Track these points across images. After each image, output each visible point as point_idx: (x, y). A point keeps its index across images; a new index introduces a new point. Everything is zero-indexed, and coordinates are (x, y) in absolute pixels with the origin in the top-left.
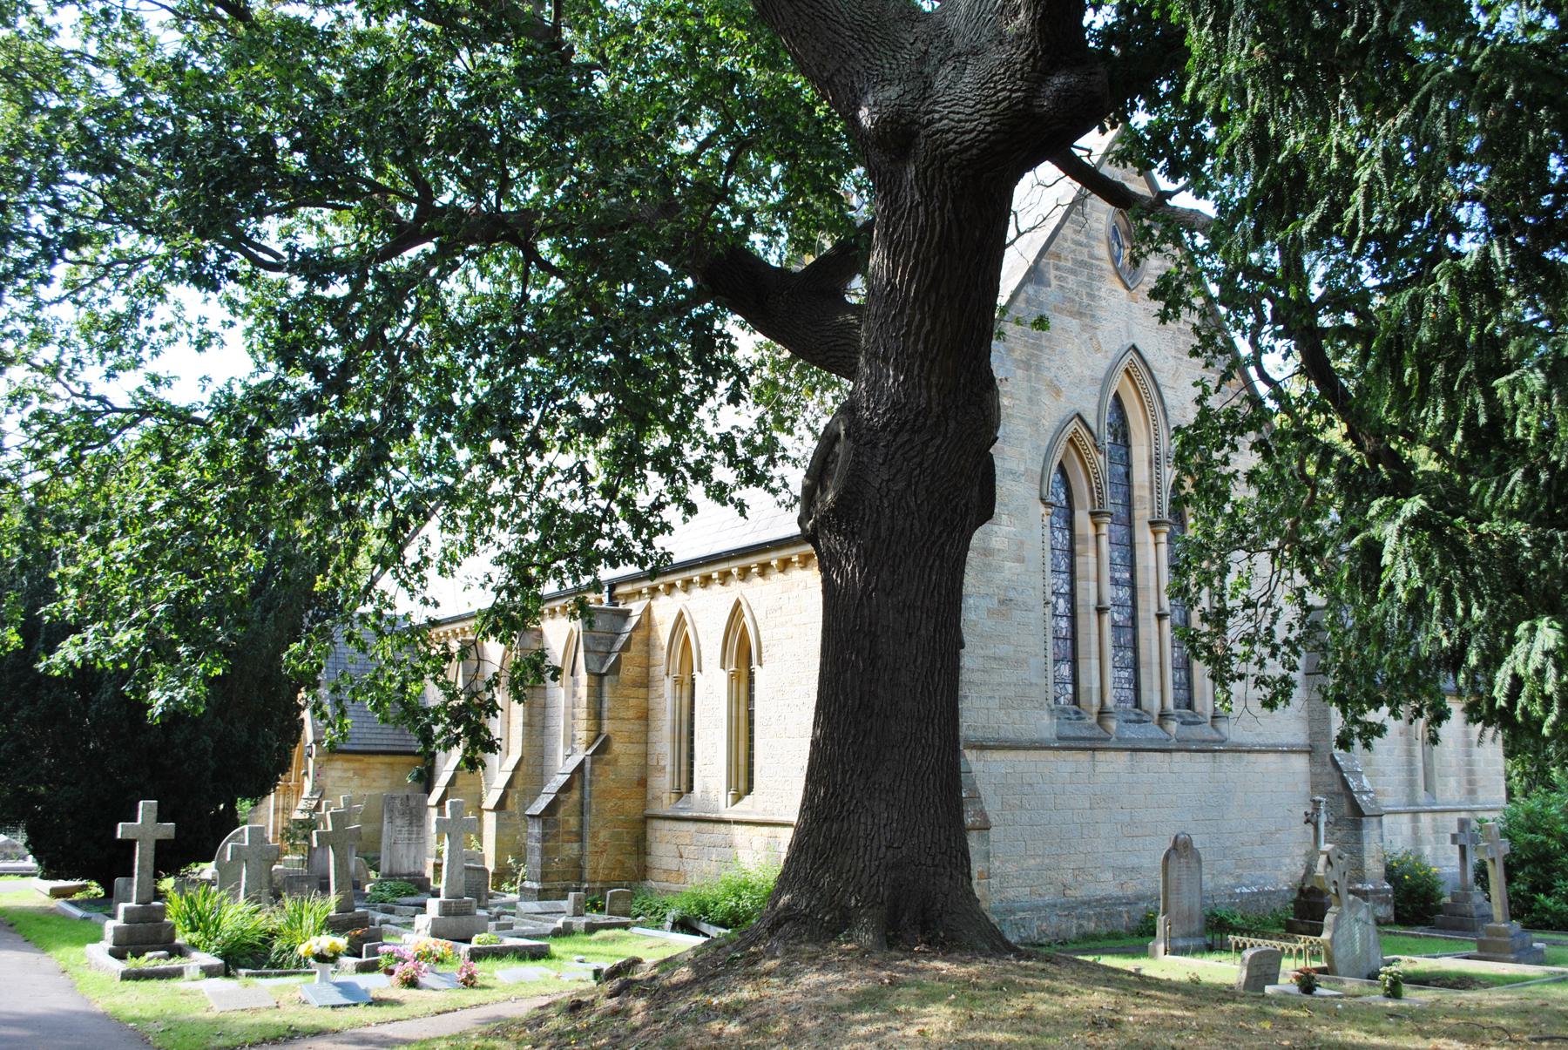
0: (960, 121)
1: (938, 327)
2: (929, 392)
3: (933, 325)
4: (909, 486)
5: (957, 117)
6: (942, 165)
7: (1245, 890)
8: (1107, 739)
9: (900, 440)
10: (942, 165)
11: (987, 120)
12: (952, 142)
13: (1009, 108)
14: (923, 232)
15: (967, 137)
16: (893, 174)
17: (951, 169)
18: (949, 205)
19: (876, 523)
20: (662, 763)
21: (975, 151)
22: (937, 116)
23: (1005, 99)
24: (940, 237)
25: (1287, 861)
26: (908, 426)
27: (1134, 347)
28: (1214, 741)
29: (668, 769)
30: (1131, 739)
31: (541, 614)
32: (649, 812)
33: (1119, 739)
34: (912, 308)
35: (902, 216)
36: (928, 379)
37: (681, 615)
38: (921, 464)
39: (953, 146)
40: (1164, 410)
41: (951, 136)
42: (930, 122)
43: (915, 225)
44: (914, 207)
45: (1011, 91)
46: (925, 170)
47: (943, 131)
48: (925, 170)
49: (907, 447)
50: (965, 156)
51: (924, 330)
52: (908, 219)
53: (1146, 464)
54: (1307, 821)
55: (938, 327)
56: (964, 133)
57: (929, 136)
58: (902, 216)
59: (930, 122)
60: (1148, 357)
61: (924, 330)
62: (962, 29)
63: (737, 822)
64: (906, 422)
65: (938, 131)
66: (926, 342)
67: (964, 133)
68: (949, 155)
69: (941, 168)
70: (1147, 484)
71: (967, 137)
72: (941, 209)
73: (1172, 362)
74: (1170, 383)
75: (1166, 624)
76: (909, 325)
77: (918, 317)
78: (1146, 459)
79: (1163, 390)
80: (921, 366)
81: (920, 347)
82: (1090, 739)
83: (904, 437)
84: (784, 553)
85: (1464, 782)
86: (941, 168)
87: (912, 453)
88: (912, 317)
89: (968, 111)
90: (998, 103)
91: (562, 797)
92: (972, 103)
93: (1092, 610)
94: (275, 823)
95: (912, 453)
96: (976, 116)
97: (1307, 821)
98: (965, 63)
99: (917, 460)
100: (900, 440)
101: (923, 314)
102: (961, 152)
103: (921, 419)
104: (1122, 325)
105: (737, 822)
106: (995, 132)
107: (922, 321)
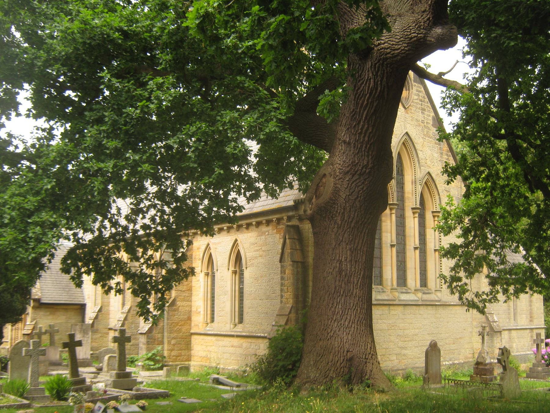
0: (393, 45)
1: (374, 131)
2: (368, 158)
3: (372, 130)
4: (358, 197)
5: (392, 43)
6: (383, 62)
7: (447, 363)
8: (395, 300)
9: (354, 178)
10: (383, 62)
11: (405, 45)
12: (389, 53)
13: (417, 40)
14: (372, 91)
15: (396, 52)
16: (360, 65)
17: (387, 64)
18: (385, 79)
19: (343, 213)
20: (199, 310)
21: (399, 57)
22: (382, 42)
23: (415, 37)
24: (379, 93)
25: (463, 351)
26: (358, 172)
27: (407, 133)
28: (436, 301)
29: (202, 313)
30: (404, 300)
31: (28, 230)
32: (192, 331)
33: (400, 300)
34: (364, 122)
35: (363, 83)
36: (368, 152)
37: (208, 245)
38: (363, 189)
39: (389, 55)
40: (419, 160)
41: (389, 50)
42: (379, 44)
43: (369, 87)
44: (369, 79)
45: (418, 34)
46: (376, 64)
47: (385, 48)
48: (376, 64)
49: (357, 181)
50: (395, 59)
51: (369, 132)
52: (366, 84)
53: (410, 183)
54: (480, 335)
55: (374, 131)
56: (394, 50)
57: (378, 50)
58: (363, 83)
59: (379, 44)
60: (412, 137)
61: (369, 132)
62: (393, 5)
63: (232, 336)
64: (358, 170)
65: (383, 48)
66: (369, 137)
67: (394, 50)
68: (387, 59)
69: (383, 64)
70: (411, 192)
71: (396, 52)
72: (381, 81)
73: (422, 140)
74: (421, 149)
75: (394, 249)
76: (362, 129)
77: (366, 126)
78: (411, 181)
79: (419, 152)
80: (366, 147)
81: (366, 139)
82: (388, 300)
83: (356, 177)
84: (259, 219)
85: (529, 317)
86: (383, 64)
87: (360, 184)
88: (363, 126)
89: (397, 40)
90: (411, 38)
91: (96, 320)
92: (399, 37)
93: (389, 245)
94: (12, 335)
95: (360, 184)
96: (401, 43)
97: (480, 335)
98: (395, 20)
99: (361, 187)
100: (354, 178)
101: (368, 125)
102: (393, 57)
103: (364, 169)
104: (402, 123)
105: (232, 336)
106: (408, 50)
107: (368, 128)
